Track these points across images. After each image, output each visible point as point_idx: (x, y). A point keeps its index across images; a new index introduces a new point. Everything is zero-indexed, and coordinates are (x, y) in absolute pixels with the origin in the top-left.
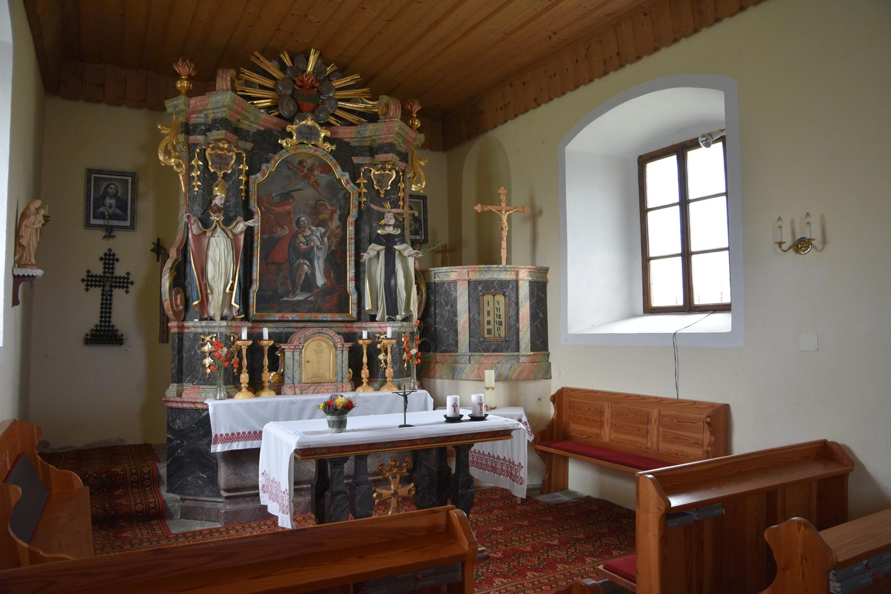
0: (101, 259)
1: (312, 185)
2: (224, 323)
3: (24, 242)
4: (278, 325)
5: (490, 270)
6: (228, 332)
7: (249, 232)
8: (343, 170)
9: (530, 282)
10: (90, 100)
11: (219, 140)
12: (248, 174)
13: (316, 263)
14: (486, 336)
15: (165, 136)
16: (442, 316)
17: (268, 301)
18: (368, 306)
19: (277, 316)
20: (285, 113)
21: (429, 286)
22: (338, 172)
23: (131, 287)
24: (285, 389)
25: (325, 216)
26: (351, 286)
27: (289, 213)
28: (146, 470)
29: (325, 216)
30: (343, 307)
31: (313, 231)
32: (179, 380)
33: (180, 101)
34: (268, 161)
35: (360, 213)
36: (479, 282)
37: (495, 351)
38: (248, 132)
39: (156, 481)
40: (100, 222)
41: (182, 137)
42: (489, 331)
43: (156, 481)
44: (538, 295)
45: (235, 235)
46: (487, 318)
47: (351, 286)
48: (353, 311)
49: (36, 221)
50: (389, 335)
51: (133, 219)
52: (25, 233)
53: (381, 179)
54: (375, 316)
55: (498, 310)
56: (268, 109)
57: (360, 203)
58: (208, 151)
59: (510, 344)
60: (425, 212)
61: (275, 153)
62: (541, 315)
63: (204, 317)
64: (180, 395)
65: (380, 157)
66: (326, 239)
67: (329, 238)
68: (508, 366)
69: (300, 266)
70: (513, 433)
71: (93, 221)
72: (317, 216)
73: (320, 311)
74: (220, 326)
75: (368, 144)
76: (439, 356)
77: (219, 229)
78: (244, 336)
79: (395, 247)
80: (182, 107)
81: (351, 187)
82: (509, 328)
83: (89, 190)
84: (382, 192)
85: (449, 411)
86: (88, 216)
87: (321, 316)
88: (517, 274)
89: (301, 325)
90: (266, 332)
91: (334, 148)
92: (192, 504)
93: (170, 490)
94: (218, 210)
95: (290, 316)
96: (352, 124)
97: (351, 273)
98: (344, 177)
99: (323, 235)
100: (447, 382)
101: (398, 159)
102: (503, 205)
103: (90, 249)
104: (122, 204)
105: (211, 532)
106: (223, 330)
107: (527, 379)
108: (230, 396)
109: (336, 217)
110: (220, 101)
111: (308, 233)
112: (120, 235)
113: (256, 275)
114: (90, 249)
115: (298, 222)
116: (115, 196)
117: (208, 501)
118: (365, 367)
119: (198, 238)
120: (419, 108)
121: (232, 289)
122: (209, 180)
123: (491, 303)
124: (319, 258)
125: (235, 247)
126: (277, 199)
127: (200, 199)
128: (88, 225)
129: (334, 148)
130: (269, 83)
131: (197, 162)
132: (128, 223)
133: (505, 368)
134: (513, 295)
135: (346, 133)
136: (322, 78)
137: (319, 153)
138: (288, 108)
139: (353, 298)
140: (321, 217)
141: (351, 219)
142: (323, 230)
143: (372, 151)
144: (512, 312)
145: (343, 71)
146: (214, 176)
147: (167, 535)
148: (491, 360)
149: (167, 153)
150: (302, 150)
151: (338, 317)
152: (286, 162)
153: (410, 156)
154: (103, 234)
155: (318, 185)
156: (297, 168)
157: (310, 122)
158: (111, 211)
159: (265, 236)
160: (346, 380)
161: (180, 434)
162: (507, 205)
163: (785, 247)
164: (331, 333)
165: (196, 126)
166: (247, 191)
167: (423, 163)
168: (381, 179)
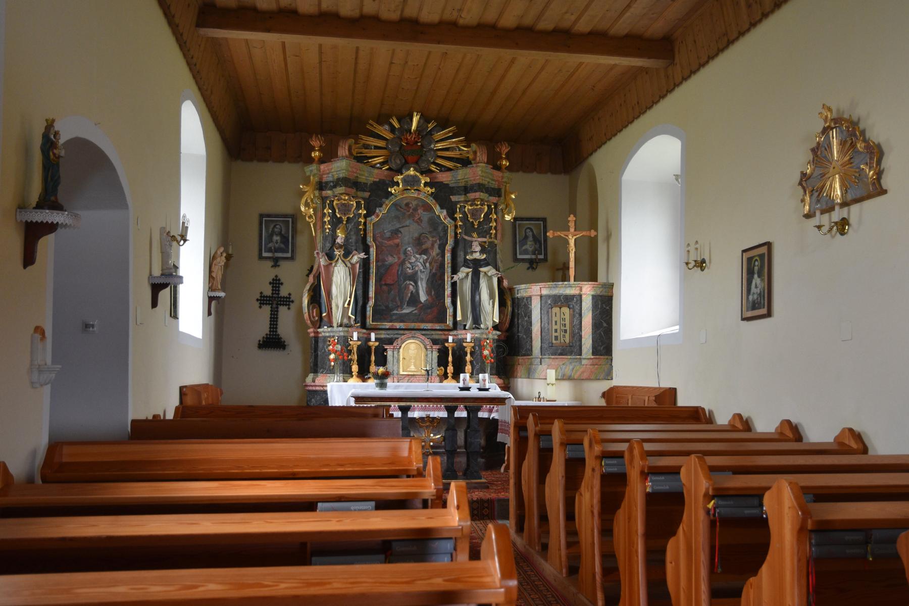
0: (270, 283)
1: (417, 222)
2: (341, 329)
3: (214, 275)
4: (389, 332)
5: (556, 287)
6: (346, 334)
7: (365, 263)
8: (442, 208)
9: (594, 297)
10: (260, 160)
11: (342, 194)
12: (366, 216)
13: (419, 284)
14: (554, 342)
16: (523, 326)
18: (459, 318)
19: (388, 325)
20: (394, 166)
21: (513, 300)
22: (437, 209)
23: (292, 305)
26: (448, 301)
27: (398, 245)
29: (428, 244)
30: (442, 318)
31: (417, 259)
33: (314, 167)
34: (381, 206)
35: (456, 241)
37: (561, 354)
38: (366, 184)
40: (270, 255)
41: (317, 193)
42: (556, 338)
44: (602, 307)
45: (353, 265)
47: (448, 301)
48: (449, 322)
49: (221, 261)
50: (469, 340)
52: (215, 269)
53: (475, 214)
54: (465, 326)
55: (564, 320)
56: (382, 164)
57: (456, 234)
58: (335, 203)
61: (387, 198)
62: (605, 325)
65: (471, 196)
66: (428, 265)
67: (430, 264)
68: (571, 367)
69: (407, 287)
70: (507, 401)
71: (519, 257)
72: (420, 245)
73: (423, 321)
75: (463, 184)
76: (520, 359)
77: (340, 261)
79: (481, 269)
80: (315, 171)
81: (448, 222)
82: (573, 335)
83: (261, 230)
84: (476, 223)
85: (461, 385)
86: (260, 250)
88: (581, 290)
89: (402, 332)
90: (373, 336)
91: (433, 190)
94: (340, 247)
95: (398, 325)
96: (449, 170)
97: (448, 291)
98: (443, 214)
99: (425, 262)
100: (525, 381)
101: (487, 195)
102: (572, 230)
104: (285, 240)
106: (342, 334)
107: (589, 379)
108: (345, 381)
109: (436, 246)
110: (339, 167)
111: (413, 260)
112: (284, 265)
113: (372, 294)
114: (261, 276)
115: (405, 253)
116: (280, 234)
118: (450, 365)
120: (507, 150)
121: (349, 304)
122: (336, 222)
123: (558, 315)
124: (422, 279)
126: (388, 235)
128: (261, 257)
129: (433, 190)
130: (381, 144)
131: (327, 211)
132: (289, 255)
133: (568, 369)
134: (577, 307)
135: (444, 178)
137: (422, 196)
138: (396, 162)
139: (450, 311)
140: (424, 247)
141: (448, 247)
142: (425, 257)
143: (466, 190)
144: (576, 322)
145: (443, 125)
146: (340, 220)
148: (557, 362)
149: (307, 205)
151: (437, 326)
152: (395, 205)
153: (503, 191)
154: (273, 264)
155: (421, 221)
156: (404, 210)
157: (412, 172)
158: (277, 246)
159: (379, 264)
162: (575, 230)
163: (691, 266)
164: (423, 337)
165: (327, 183)
166: (365, 230)
167: (513, 197)
168: (475, 214)
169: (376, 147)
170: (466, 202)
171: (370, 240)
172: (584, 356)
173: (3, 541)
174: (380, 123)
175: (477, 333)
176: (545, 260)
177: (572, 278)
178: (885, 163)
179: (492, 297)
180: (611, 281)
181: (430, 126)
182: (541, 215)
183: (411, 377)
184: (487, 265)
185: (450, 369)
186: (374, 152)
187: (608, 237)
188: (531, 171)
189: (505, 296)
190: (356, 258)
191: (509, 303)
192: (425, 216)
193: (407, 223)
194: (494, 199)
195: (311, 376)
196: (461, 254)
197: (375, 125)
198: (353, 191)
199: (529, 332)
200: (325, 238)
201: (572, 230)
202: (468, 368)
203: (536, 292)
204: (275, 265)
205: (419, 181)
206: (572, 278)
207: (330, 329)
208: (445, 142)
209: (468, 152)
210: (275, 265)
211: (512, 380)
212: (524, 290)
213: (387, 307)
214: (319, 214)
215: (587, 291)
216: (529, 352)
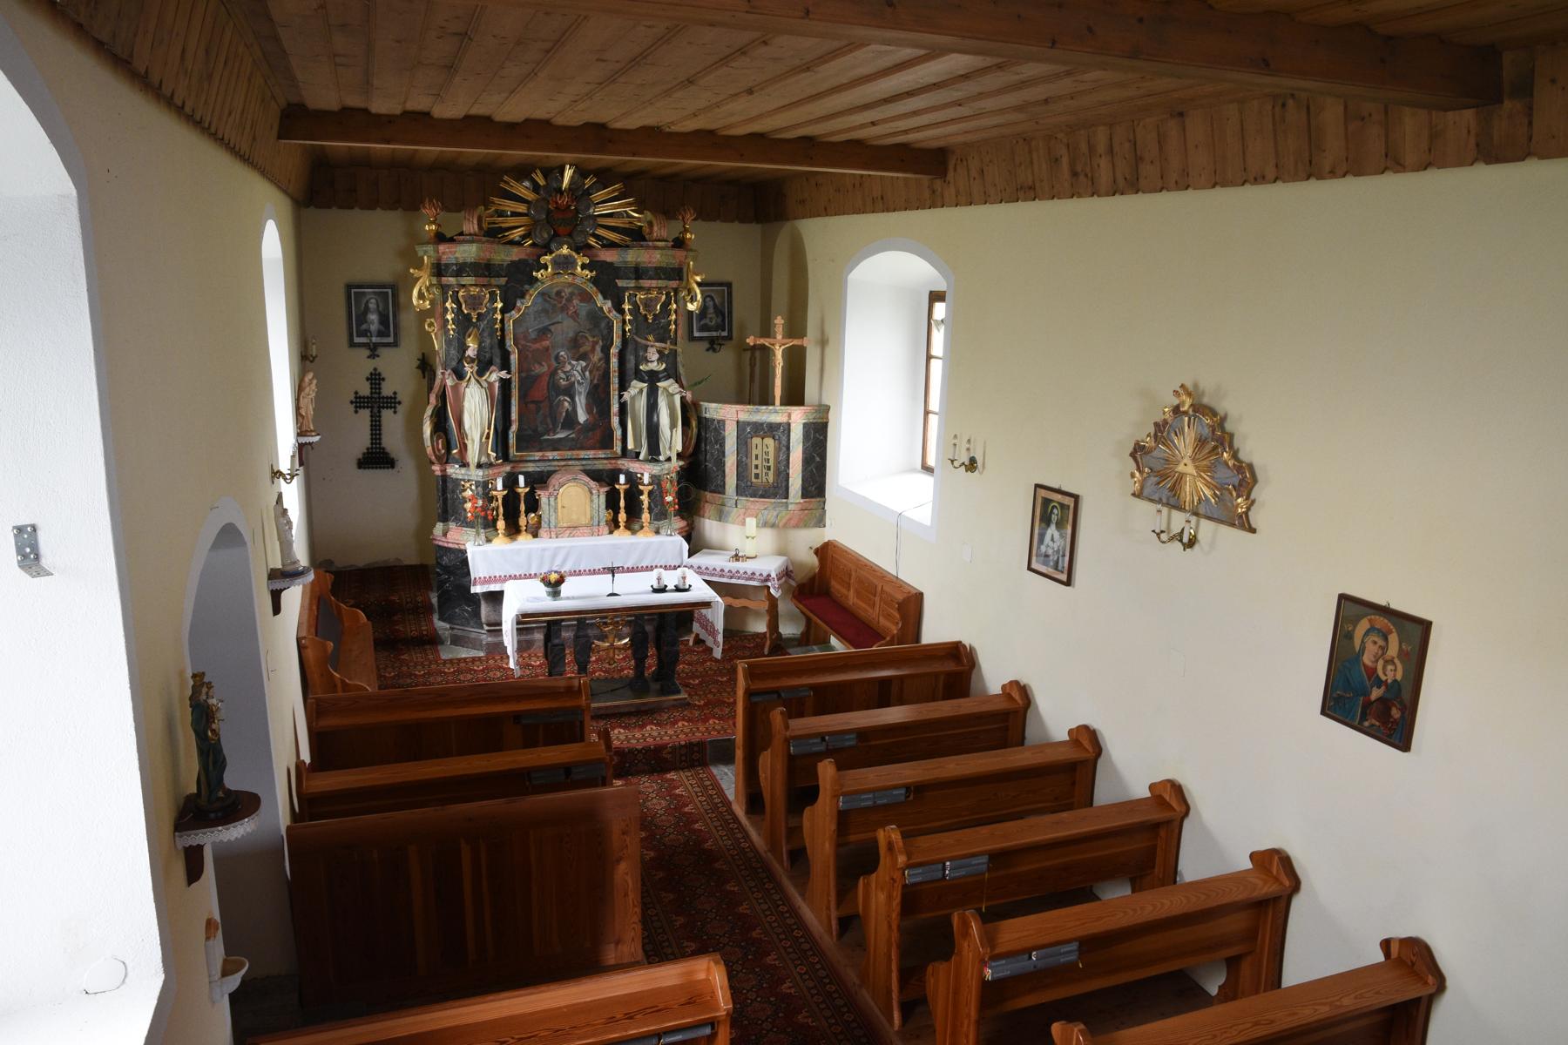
2: (480, 472)
3: (303, 412)
5: (758, 411)
7: (505, 385)
12: (503, 311)
15: (418, 279)
17: (528, 440)
18: (630, 446)
19: (537, 455)
21: (700, 420)
22: (599, 299)
24: (541, 532)
25: (586, 348)
26: (615, 421)
28: (419, 599)
29: (586, 348)
30: (606, 442)
32: (445, 520)
34: (523, 296)
36: (749, 424)
39: (429, 609)
41: (434, 280)
43: (429, 609)
45: (491, 385)
46: (755, 462)
47: (615, 421)
48: (618, 448)
49: (311, 390)
51: (396, 335)
53: (648, 304)
55: (767, 453)
56: (524, 237)
57: (624, 331)
59: (779, 489)
60: (730, 303)
63: (465, 465)
64: (445, 535)
65: (646, 283)
71: (357, 340)
73: (582, 448)
74: (478, 475)
76: (709, 495)
78: (500, 486)
82: (778, 473)
84: (650, 317)
87: (583, 454)
92: (460, 633)
93: (441, 619)
94: (472, 361)
95: (550, 455)
97: (615, 408)
98: (607, 306)
100: (715, 523)
102: (779, 337)
103: (355, 370)
105: (474, 660)
107: (797, 526)
108: (489, 541)
109: (598, 348)
111: (568, 368)
113: (514, 416)
114: (355, 370)
115: (557, 357)
117: (473, 632)
119: (455, 388)
122: (464, 323)
125: (491, 396)
127: (455, 343)
128: (352, 345)
130: (522, 208)
132: (391, 340)
134: (784, 438)
135: (609, 256)
136: (579, 193)
137: (578, 281)
139: (618, 433)
141: (614, 351)
144: (782, 457)
147: (437, 660)
148: (758, 506)
150: (558, 280)
151: (601, 454)
152: (542, 294)
154: (368, 352)
156: (554, 302)
157: (565, 250)
160: (603, 523)
161: (446, 569)
165: (447, 265)
166: (503, 329)
168: (648, 304)
169: (514, 214)
170: (639, 289)
171: (510, 343)
172: (791, 500)
173: (143, 1041)
174: (519, 180)
175: (656, 469)
176: (730, 338)
177: (778, 401)
178: (1236, 444)
179: (673, 426)
180: (826, 401)
181: (588, 182)
182: (727, 278)
183: (573, 529)
184: (667, 378)
185: (622, 517)
186: (512, 222)
187: (823, 343)
188: (714, 220)
189: (689, 412)
190: (494, 376)
191: (694, 424)
192: (583, 309)
193: (559, 318)
194: (674, 284)
195: (439, 526)
196: (631, 360)
197: (513, 183)
198: (457, 205)
199: (721, 464)
200: (449, 342)
201: (779, 337)
202: (646, 516)
203: (729, 415)
204: (373, 356)
205: (574, 263)
206: (778, 401)
207: (463, 471)
208: (608, 207)
209: (639, 220)
210: (373, 356)
211: (696, 519)
212: (713, 410)
213: (535, 431)
214: (439, 309)
215: (797, 418)
216: (721, 489)
